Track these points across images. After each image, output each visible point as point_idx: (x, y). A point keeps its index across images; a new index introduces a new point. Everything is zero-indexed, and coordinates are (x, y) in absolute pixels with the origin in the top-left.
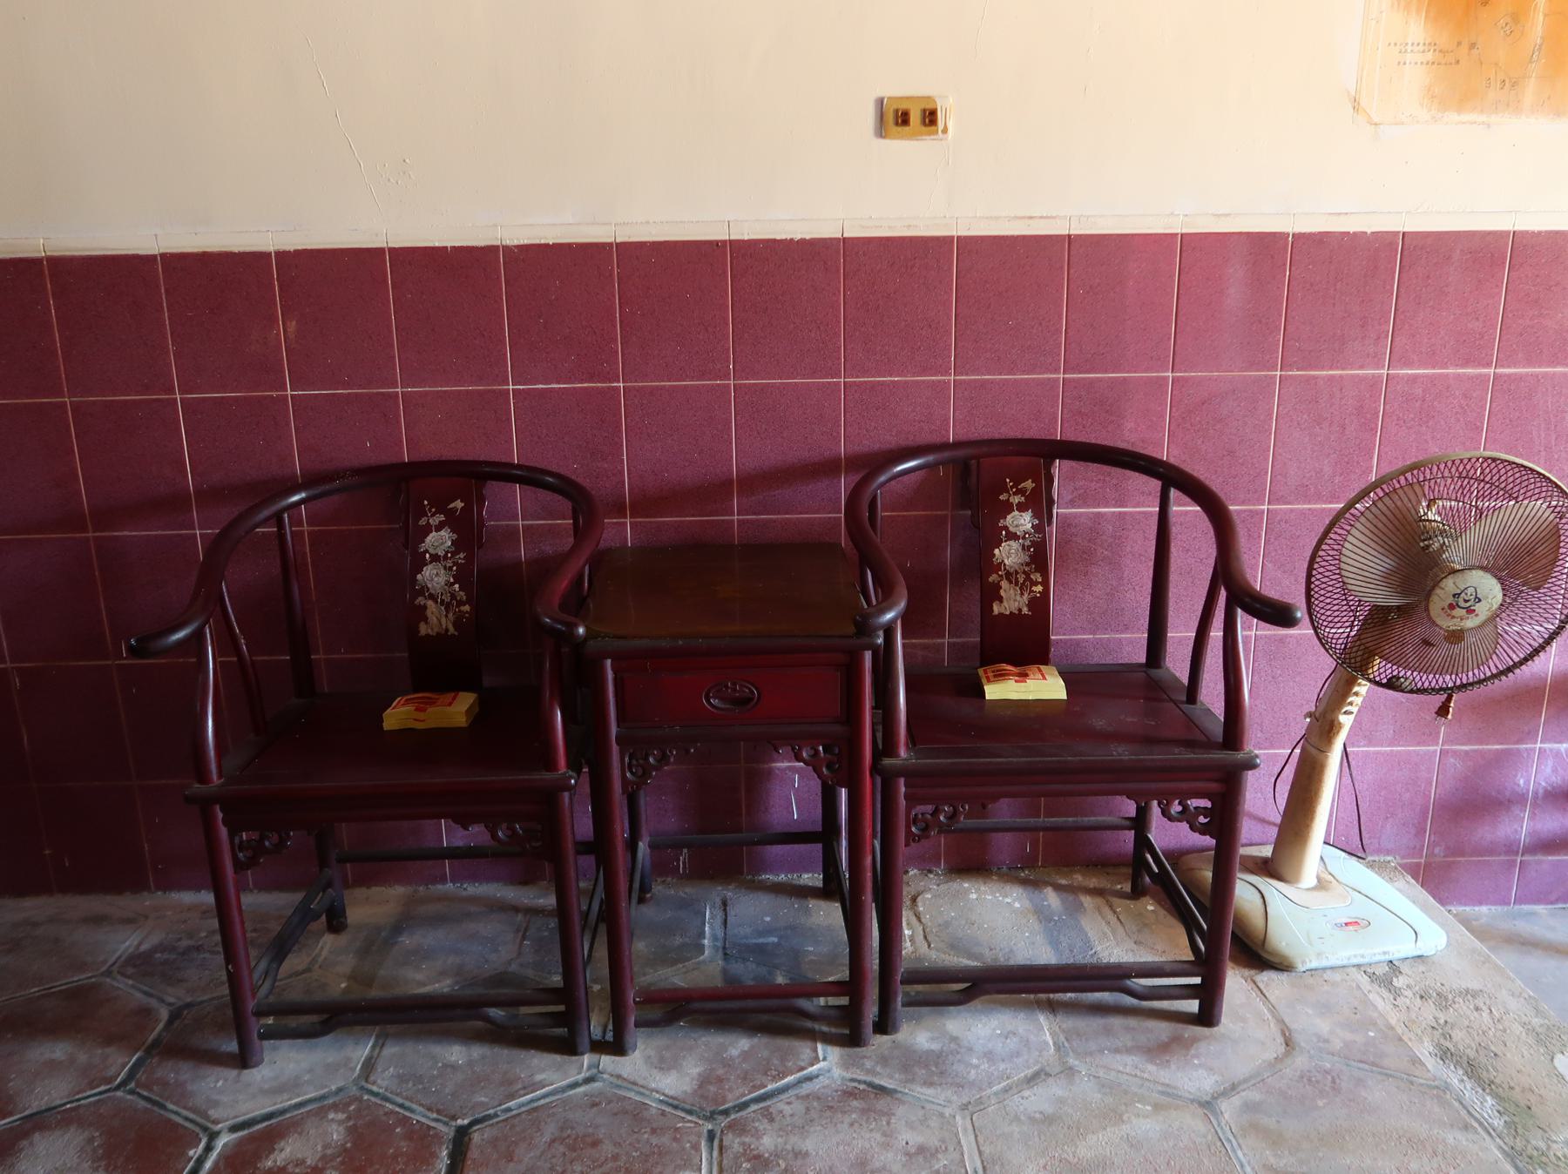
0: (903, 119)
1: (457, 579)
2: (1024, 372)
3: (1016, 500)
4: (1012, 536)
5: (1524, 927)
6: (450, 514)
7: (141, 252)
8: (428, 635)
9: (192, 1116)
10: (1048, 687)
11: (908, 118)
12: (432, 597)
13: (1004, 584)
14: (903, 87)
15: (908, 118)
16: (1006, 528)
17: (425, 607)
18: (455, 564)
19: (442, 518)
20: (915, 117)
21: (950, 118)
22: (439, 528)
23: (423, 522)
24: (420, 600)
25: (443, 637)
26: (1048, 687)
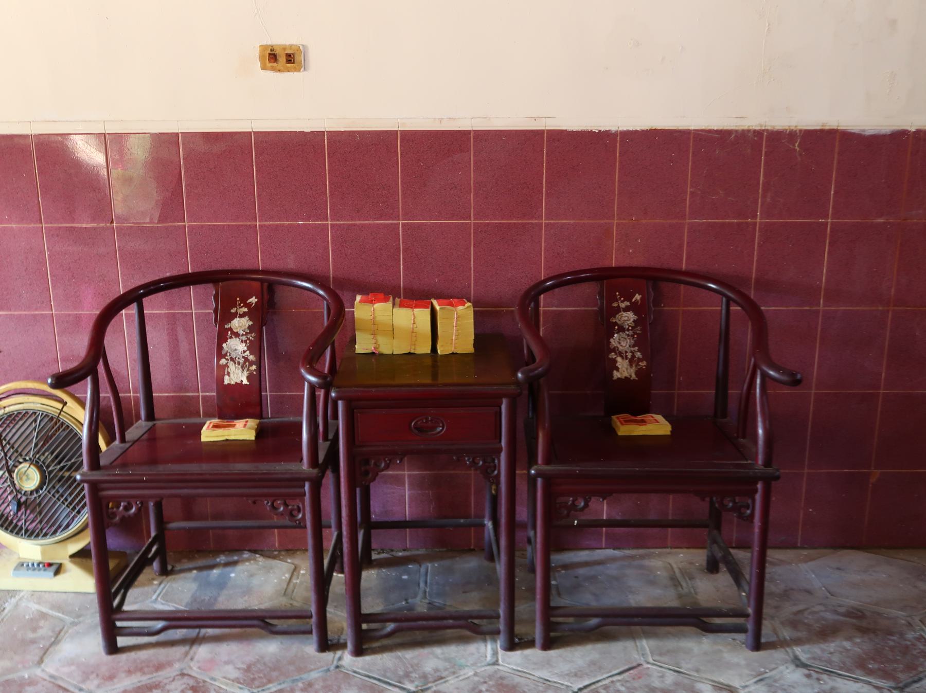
0: (290, 58)
1: (249, 348)
2: (283, 226)
3: (623, 305)
4: (622, 329)
5: (232, 600)
6: (248, 305)
7: (570, 129)
8: (619, 379)
9: (528, 676)
10: (658, 426)
11: (283, 58)
12: (620, 354)
13: (619, 359)
14: (282, 39)
15: (283, 58)
16: (231, 329)
17: (615, 361)
18: (635, 333)
19: (246, 310)
20: (282, 59)
21: (314, 57)
22: (242, 316)
23: (233, 311)
24: (612, 355)
25: (239, 385)
26: (658, 426)
